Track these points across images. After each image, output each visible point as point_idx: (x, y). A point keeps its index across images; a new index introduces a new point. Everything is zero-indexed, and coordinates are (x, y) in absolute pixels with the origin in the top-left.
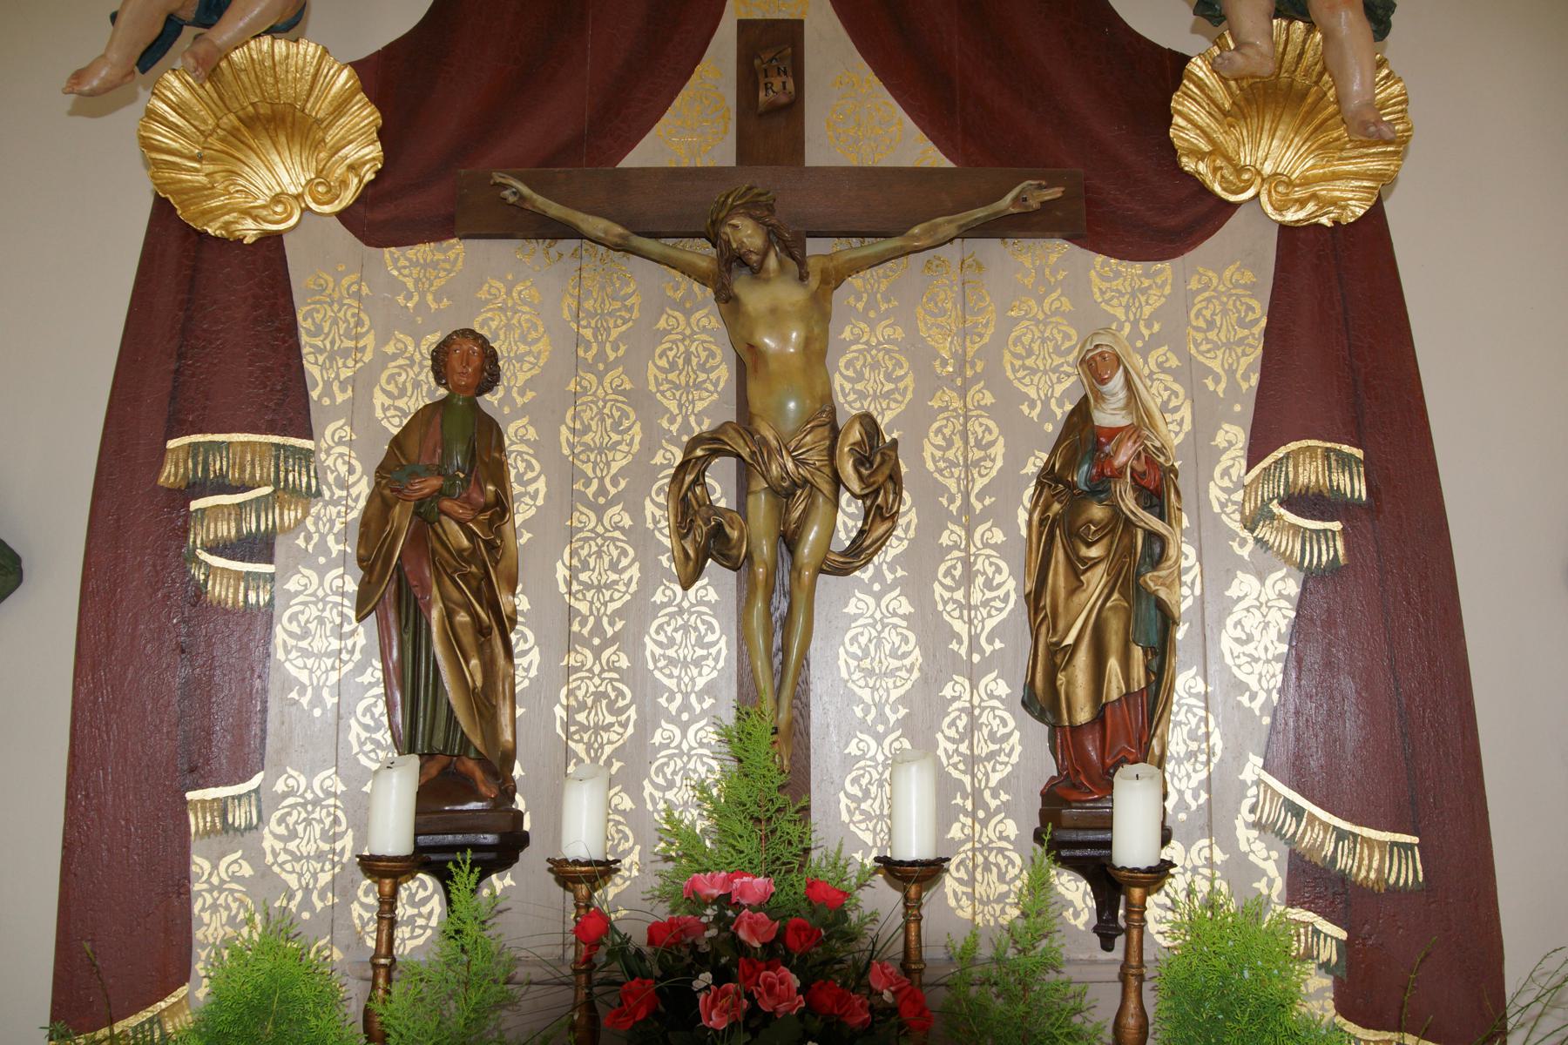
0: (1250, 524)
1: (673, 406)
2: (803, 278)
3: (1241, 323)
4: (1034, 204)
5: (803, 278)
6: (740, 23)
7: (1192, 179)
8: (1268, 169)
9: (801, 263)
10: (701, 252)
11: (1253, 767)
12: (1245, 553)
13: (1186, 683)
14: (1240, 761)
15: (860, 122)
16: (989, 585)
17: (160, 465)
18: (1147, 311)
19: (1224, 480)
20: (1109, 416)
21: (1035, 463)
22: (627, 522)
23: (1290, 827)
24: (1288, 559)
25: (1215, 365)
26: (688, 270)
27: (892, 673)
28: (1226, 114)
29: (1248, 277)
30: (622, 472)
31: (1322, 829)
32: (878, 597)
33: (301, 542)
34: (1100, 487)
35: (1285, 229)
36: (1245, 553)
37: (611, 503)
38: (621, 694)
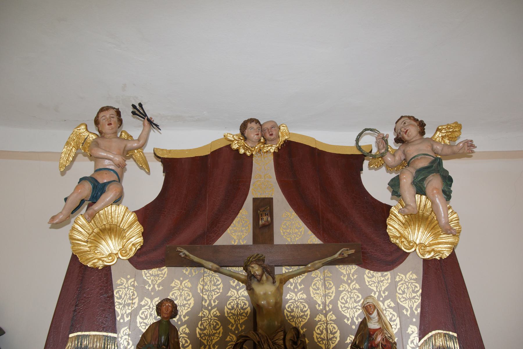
6: (255, 200)
7: (395, 245)
8: (418, 242)
15: (292, 229)
18: (383, 288)
20: (373, 325)
25: (406, 306)
26: (239, 279)
28: (403, 224)
29: (415, 276)
35: (425, 260)
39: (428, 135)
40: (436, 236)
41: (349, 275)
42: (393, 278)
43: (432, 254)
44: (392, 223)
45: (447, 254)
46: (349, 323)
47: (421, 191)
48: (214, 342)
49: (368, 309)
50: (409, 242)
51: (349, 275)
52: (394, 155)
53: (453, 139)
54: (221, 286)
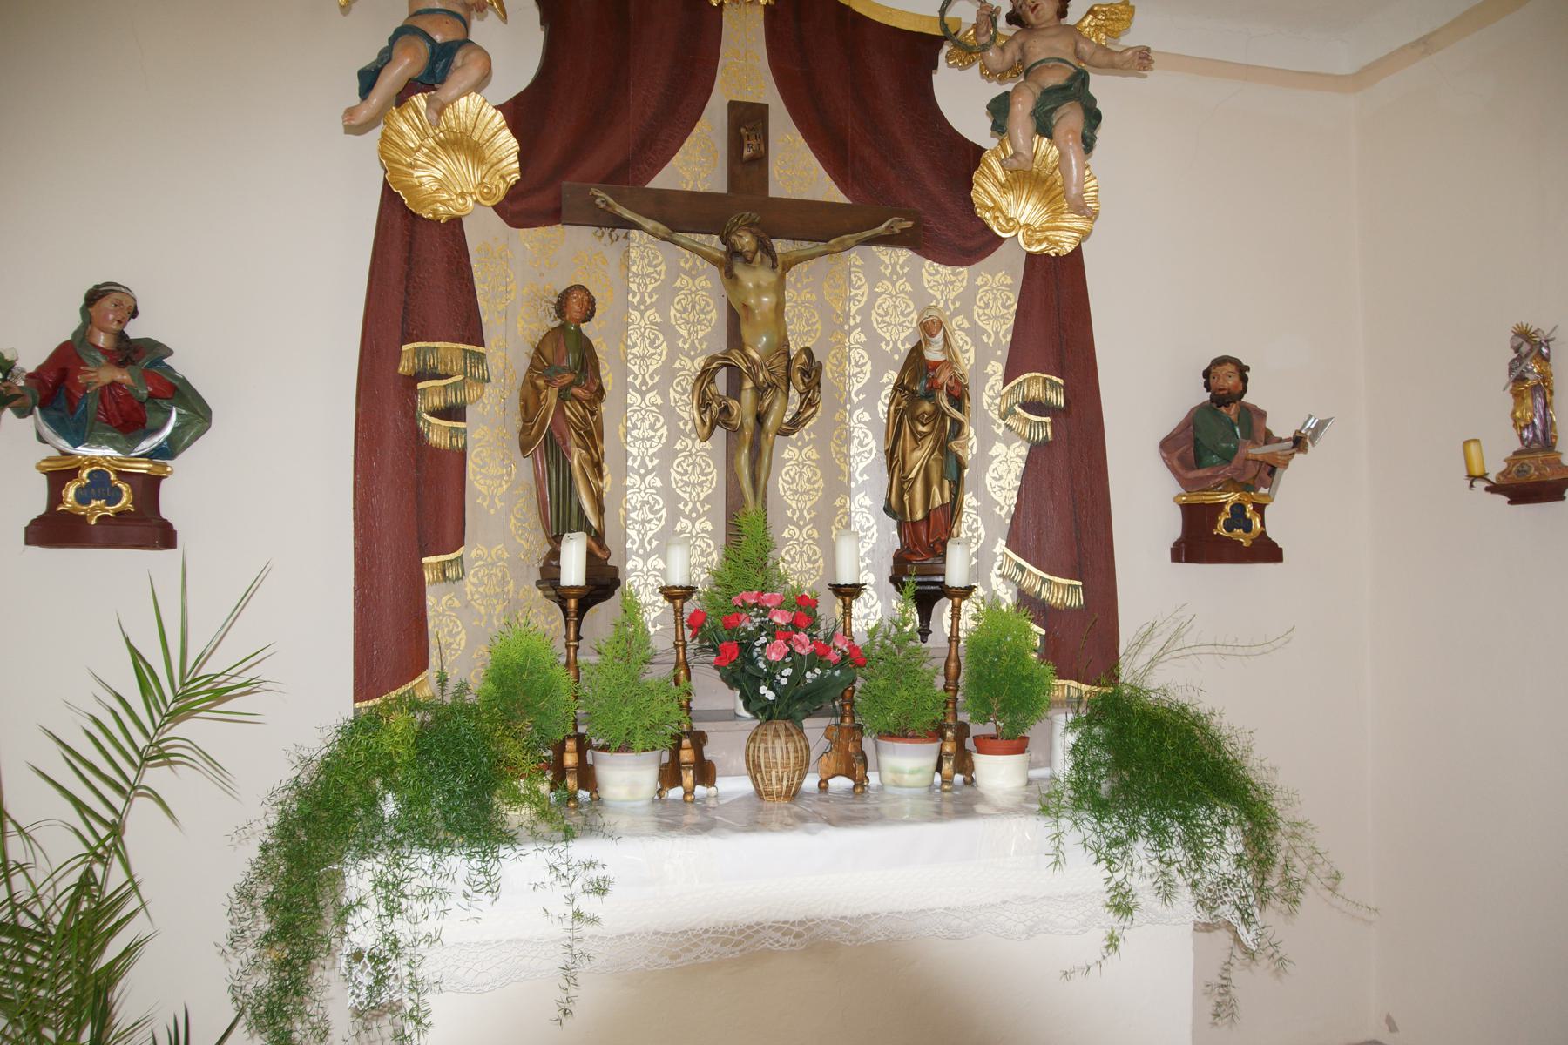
0: (1004, 417)
1: (685, 333)
2: (774, 268)
3: (1003, 305)
4: (897, 230)
5: (774, 268)
6: (733, 105)
7: (981, 221)
8: (1022, 221)
9: (774, 259)
10: (714, 243)
11: (1001, 546)
12: (1000, 432)
13: (969, 500)
14: (995, 542)
15: (797, 171)
16: (861, 444)
17: (398, 361)
18: (953, 294)
19: (991, 391)
20: (933, 354)
21: (892, 376)
22: (659, 401)
23: (1018, 577)
24: (1022, 436)
25: (989, 328)
26: (706, 257)
27: (807, 492)
28: (1002, 186)
29: (1009, 281)
30: (656, 372)
31: (1035, 578)
32: (801, 449)
33: (480, 409)
34: (930, 395)
35: (1029, 254)
36: (1000, 432)
37: (649, 390)
38: (657, 502)
39: (1072, 18)
40: (1055, 214)
41: (894, 266)
42: (972, 279)
43: (1045, 245)
44: (982, 180)
45: (1069, 248)
46: (888, 349)
47: (1044, 129)
48: (651, 369)
49: (928, 328)
50: (1008, 220)
51: (894, 266)
52: (1002, 49)
53: (1113, 35)
54: (663, 268)
